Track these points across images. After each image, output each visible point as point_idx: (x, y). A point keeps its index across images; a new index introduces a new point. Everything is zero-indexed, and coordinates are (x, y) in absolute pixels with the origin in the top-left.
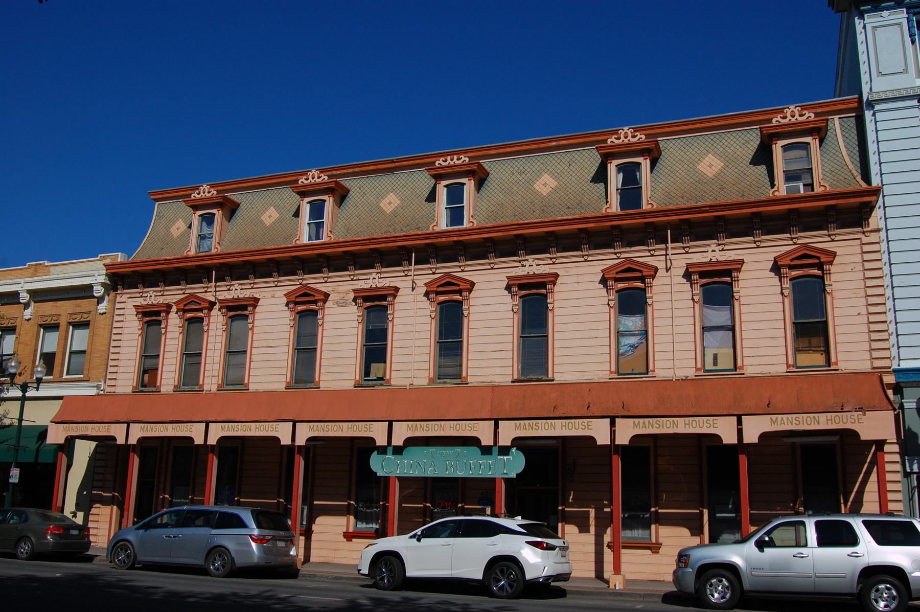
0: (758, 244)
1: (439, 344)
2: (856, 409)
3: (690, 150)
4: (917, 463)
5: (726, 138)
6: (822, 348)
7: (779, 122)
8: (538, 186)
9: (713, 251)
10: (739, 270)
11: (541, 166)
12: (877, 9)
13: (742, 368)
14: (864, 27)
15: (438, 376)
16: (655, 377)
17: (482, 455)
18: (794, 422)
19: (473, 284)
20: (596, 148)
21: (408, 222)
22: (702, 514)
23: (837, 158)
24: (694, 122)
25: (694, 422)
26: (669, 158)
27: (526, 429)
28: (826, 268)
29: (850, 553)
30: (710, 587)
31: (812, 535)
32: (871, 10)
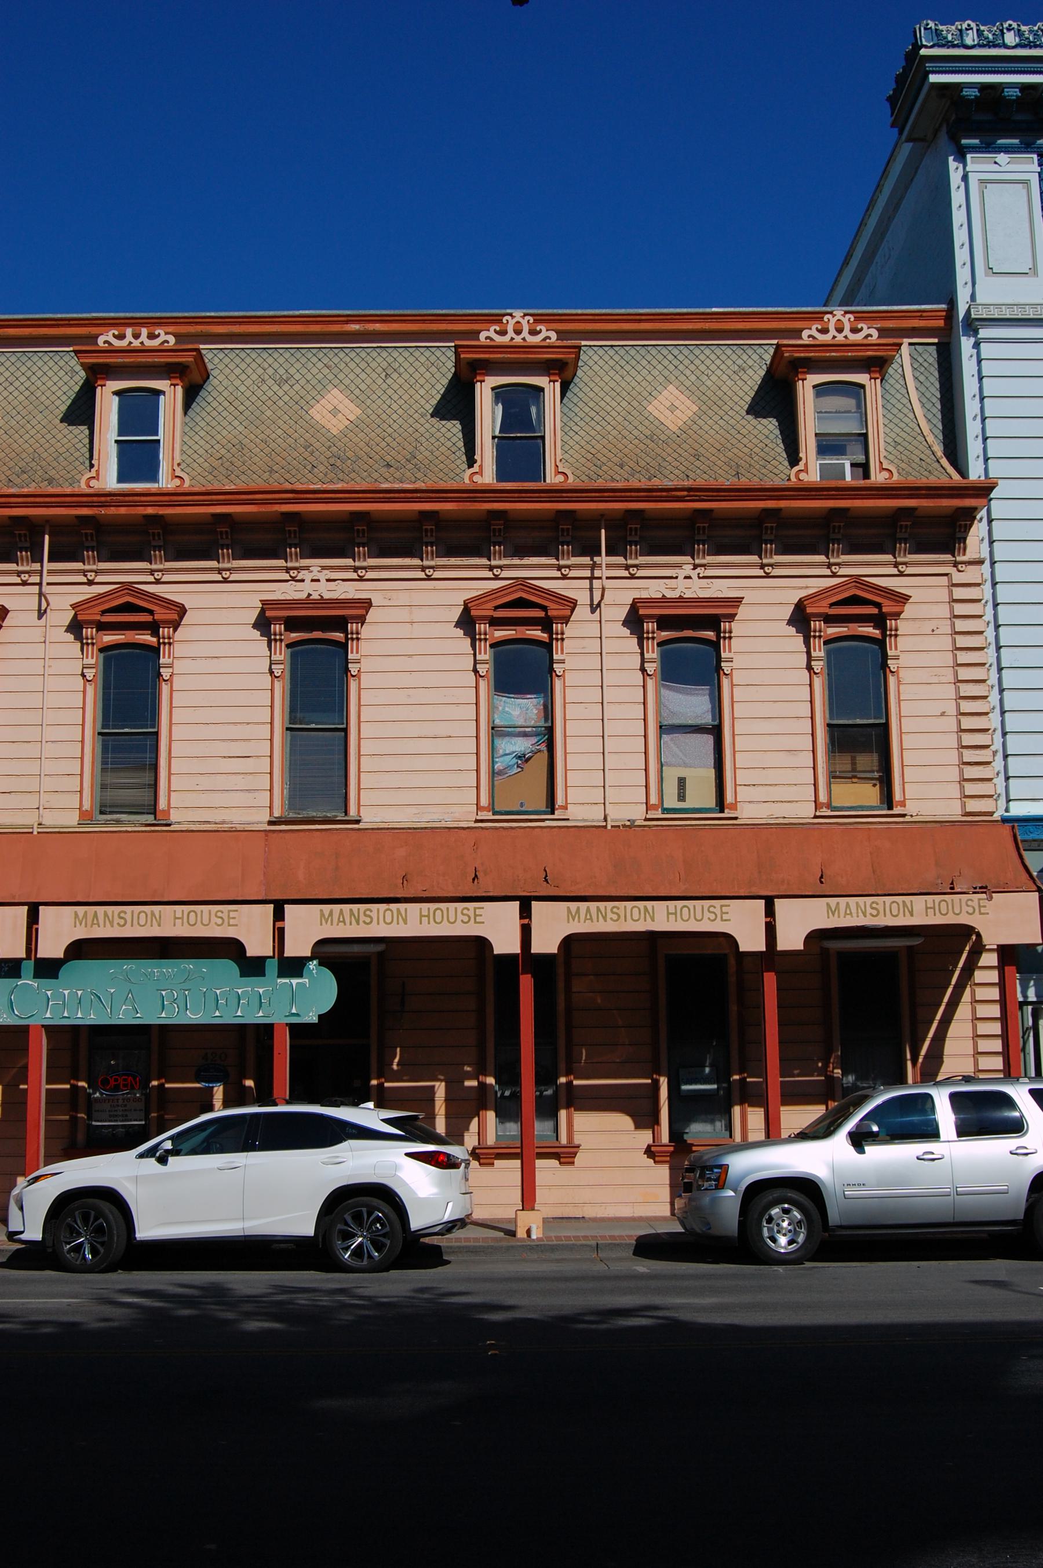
0: (767, 571)
1: (100, 736)
2: (975, 888)
3: (633, 372)
4: (1035, 985)
5: (702, 357)
6: (876, 773)
7: (814, 338)
8: (319, 413)
9: (686, 578)
10: (731, 617)
11: (326, 371)
12: (988, 147)
13: (734, 807)
14: (965, 178)
15: (101, 806)
16: (568, 819)
17: (241, 976)
18: (869, 910)
19: (182, 611)
20: (456, 347)
21: (22, 464)
22: (656, 1086)
23: (906, 420)
24: (643, 317)
25: (685, 910)
26: (592, 385)
27: (344, 922)
28: (891, 625)
29: (1013, 1148)
30: (767, 1223)
31: (945, 1116)
32: (980, 148)
